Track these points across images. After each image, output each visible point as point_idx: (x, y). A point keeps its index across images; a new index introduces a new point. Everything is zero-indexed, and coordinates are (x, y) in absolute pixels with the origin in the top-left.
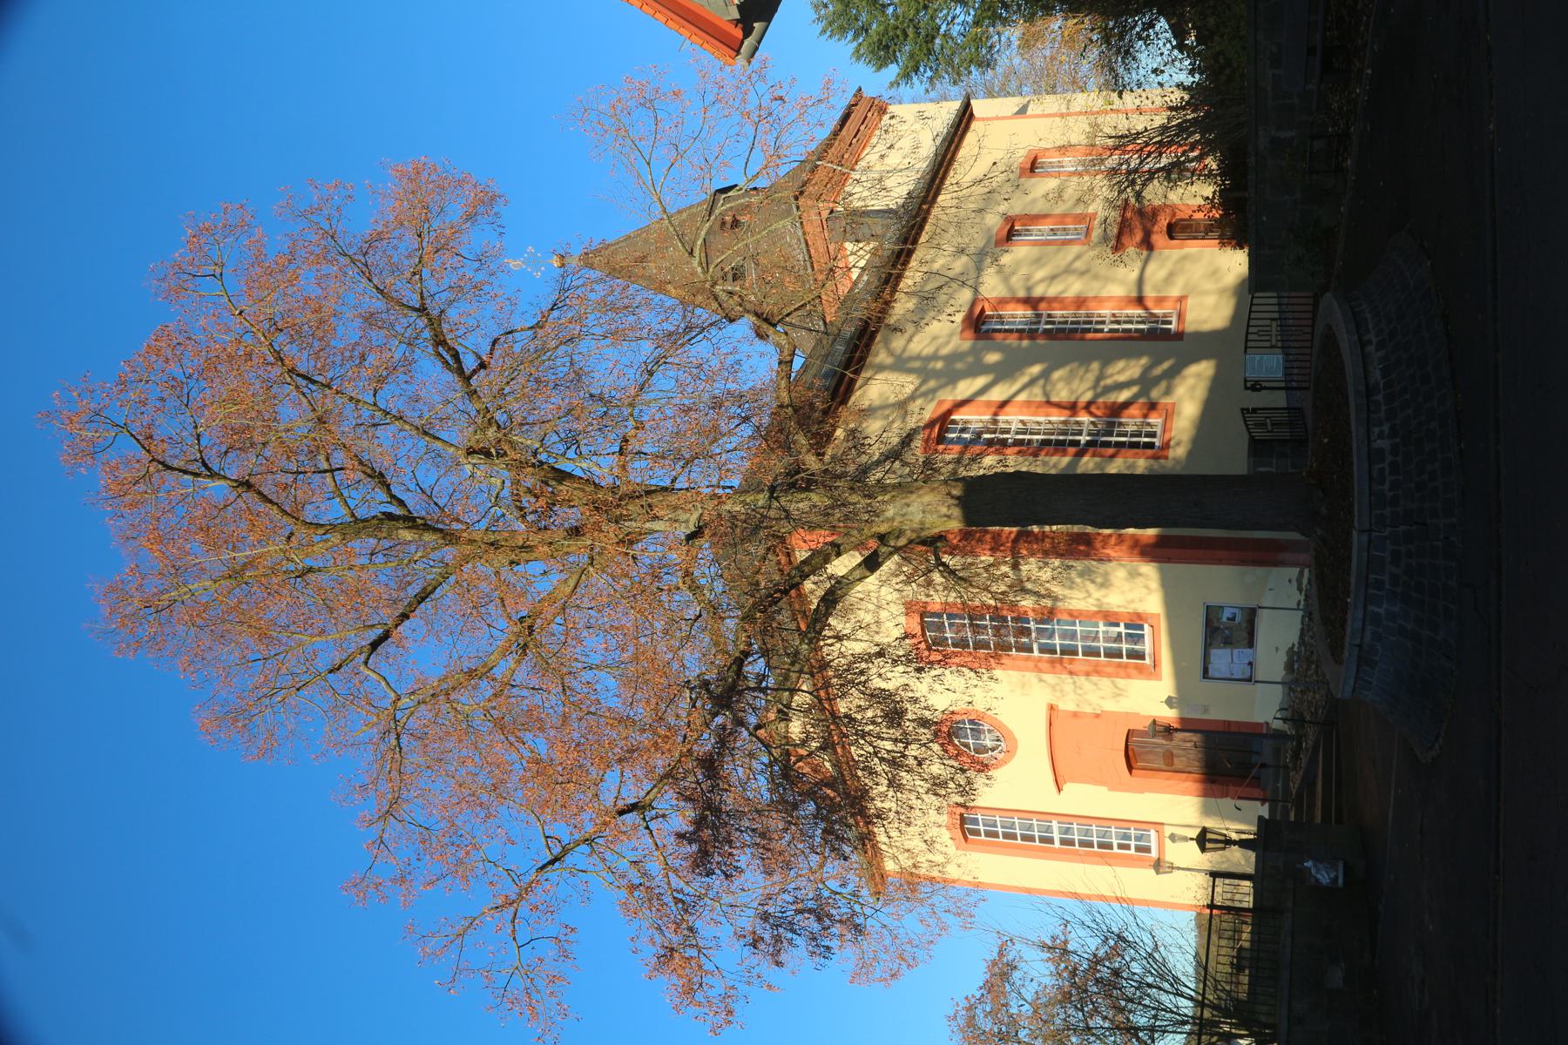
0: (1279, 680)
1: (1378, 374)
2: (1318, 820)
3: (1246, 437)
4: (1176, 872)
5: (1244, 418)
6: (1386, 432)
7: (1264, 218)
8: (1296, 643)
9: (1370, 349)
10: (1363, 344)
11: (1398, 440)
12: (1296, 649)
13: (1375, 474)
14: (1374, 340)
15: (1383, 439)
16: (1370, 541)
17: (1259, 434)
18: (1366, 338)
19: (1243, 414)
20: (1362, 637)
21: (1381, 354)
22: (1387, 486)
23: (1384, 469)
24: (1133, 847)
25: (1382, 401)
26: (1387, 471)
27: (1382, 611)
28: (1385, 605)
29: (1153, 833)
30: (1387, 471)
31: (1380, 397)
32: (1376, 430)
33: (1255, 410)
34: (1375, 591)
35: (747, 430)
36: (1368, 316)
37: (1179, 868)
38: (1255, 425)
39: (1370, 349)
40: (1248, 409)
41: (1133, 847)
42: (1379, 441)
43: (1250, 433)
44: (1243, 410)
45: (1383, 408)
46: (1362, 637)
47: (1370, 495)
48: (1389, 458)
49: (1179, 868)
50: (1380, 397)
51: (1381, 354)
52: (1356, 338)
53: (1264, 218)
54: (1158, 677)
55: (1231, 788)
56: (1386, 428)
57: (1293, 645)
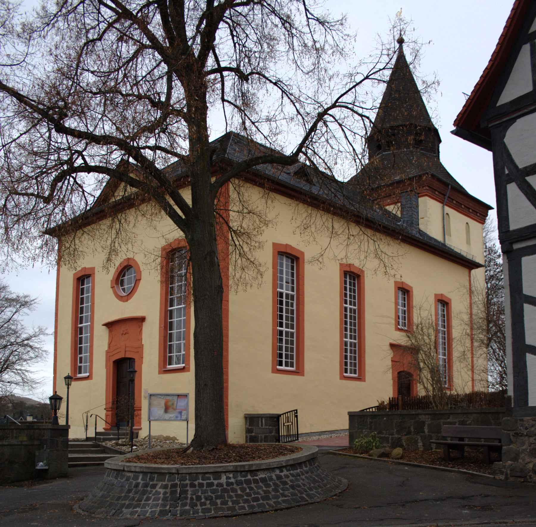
0: (151, 434)
1: (263, 476)
2: (70, 456)
3: (281, 413)
4: (66, 387)
5: (292, 411)
6: (230, 481)
7: (385, 419)
8: (179, 441)
9: (277, 472)
10: (281, 468)
11: (225, 487)
12: (176, 441)
13: (207, 475)
14: (282, 474)
15: (226, 479)
16: (173, 474)
17: (282, 420)
18: (284, 470)
19: (294, 411)
20: (128, 471)
21: (274, 477)
22: (201, 481)
23: (210, 480)
24: (81, 365)
25: (247, 478)
26: (209, 481)
27: (140, 480)
28: (142, 482)
29: (88, 374)
30: (209, 481)
31: (249, 477)
32: (231, 475)
33: (296, 416)
34: (149, 477)
35: (15, 256)
36: (298, 471)
37: (68, 388)
38: (288, 417)
39: (277, 472)
40: (297, 413)
41: (81, 365)
42: (225, 477)
43: (283, 414)
44: (297, 410)
45: (243, 479)
46: (128, 471)
47: (197, 473)
48: (216, 482)
49: (68, 388)
50: (249, 477)
51: (274, 477)
52: (284, 464)
53: (385, 419)
54: (189, 371)
55: (110, 413)
56: (233, 480)
57: (178, 440)
